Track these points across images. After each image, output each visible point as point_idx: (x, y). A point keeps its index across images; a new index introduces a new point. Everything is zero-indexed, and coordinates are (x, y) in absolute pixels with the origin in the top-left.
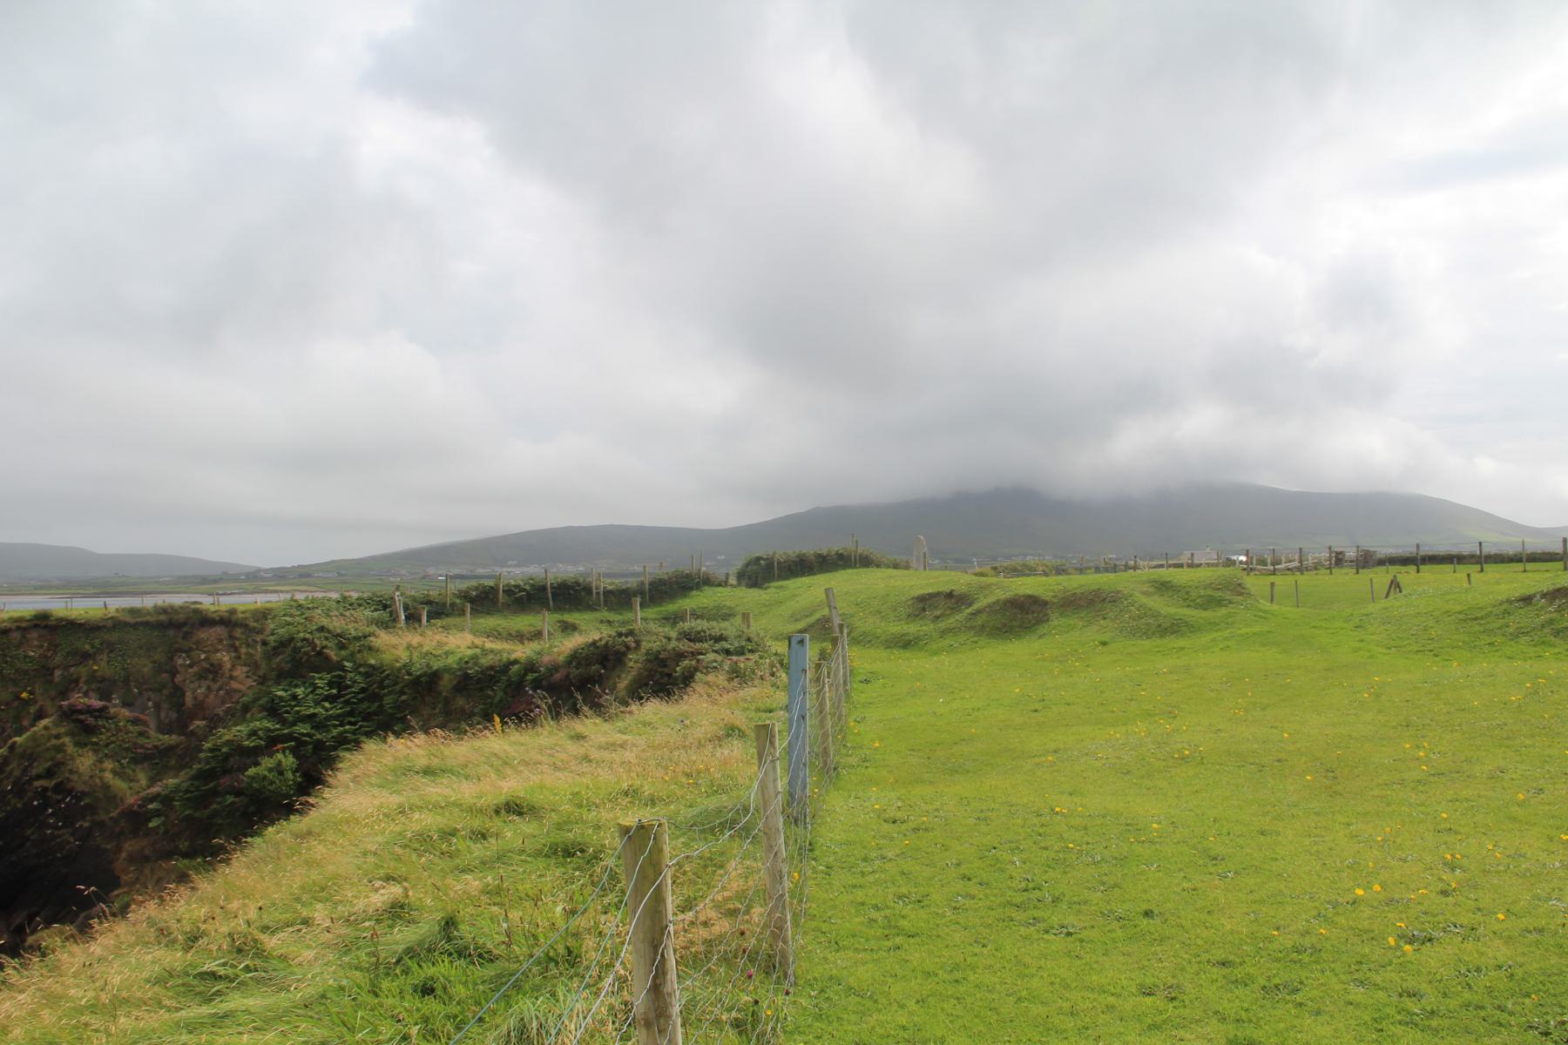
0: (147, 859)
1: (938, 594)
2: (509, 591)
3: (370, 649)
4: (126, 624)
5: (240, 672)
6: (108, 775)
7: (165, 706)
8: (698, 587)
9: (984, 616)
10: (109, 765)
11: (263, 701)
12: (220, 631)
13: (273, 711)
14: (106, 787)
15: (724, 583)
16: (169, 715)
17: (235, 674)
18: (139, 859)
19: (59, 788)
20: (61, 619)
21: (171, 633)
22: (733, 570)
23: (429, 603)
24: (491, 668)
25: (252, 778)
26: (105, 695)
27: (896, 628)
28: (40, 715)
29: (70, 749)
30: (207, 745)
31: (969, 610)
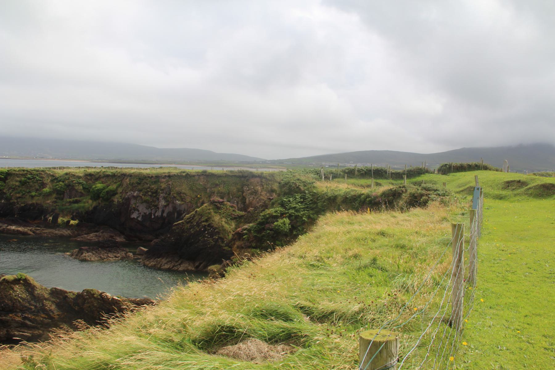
0: (243, 248)
1: (514, 181)
2: (359, 171)
3: (314, 187)
4: (229, 176)
5: (264, 193)
6: (223, 223)
7: (240, 202)
8: (424, 173)
9: (532, 190)
10: (224, 220)
11: (279, 201)
12: (258, 179)
13: (282, 205)
14: (223, 226)
15: (433, 173)
16: (241, 205)
17: (262, 194)
18: (240, 248)
19: (209, 225)
20: (210, 173)
21: (243, 179)
22: (437, 167)
23: (332, 173)
24: (355, 196)
25: (276, 225)
26: (222, 198)
27: (497, 192)
28: (203, 203)
29: (213, 214)
30: (262, 214)
31: (526, 188)
